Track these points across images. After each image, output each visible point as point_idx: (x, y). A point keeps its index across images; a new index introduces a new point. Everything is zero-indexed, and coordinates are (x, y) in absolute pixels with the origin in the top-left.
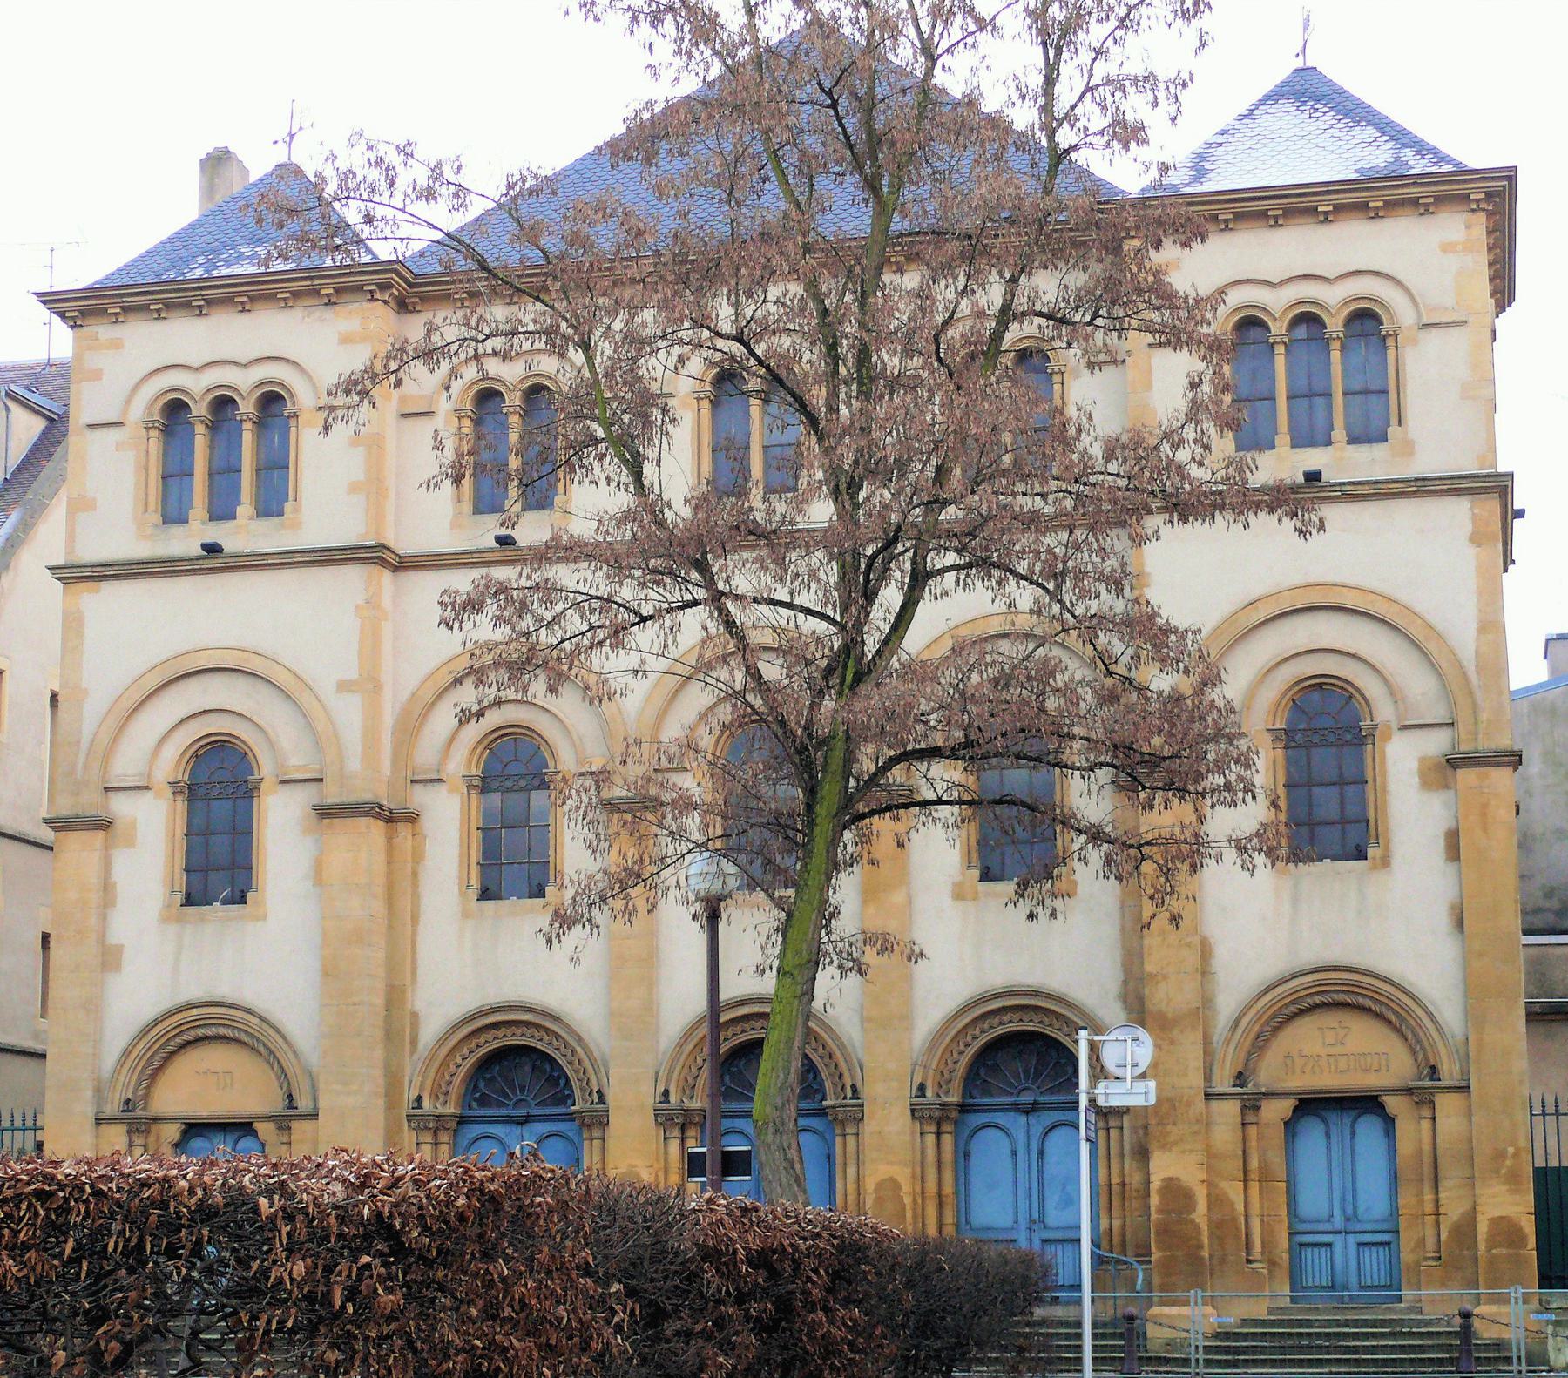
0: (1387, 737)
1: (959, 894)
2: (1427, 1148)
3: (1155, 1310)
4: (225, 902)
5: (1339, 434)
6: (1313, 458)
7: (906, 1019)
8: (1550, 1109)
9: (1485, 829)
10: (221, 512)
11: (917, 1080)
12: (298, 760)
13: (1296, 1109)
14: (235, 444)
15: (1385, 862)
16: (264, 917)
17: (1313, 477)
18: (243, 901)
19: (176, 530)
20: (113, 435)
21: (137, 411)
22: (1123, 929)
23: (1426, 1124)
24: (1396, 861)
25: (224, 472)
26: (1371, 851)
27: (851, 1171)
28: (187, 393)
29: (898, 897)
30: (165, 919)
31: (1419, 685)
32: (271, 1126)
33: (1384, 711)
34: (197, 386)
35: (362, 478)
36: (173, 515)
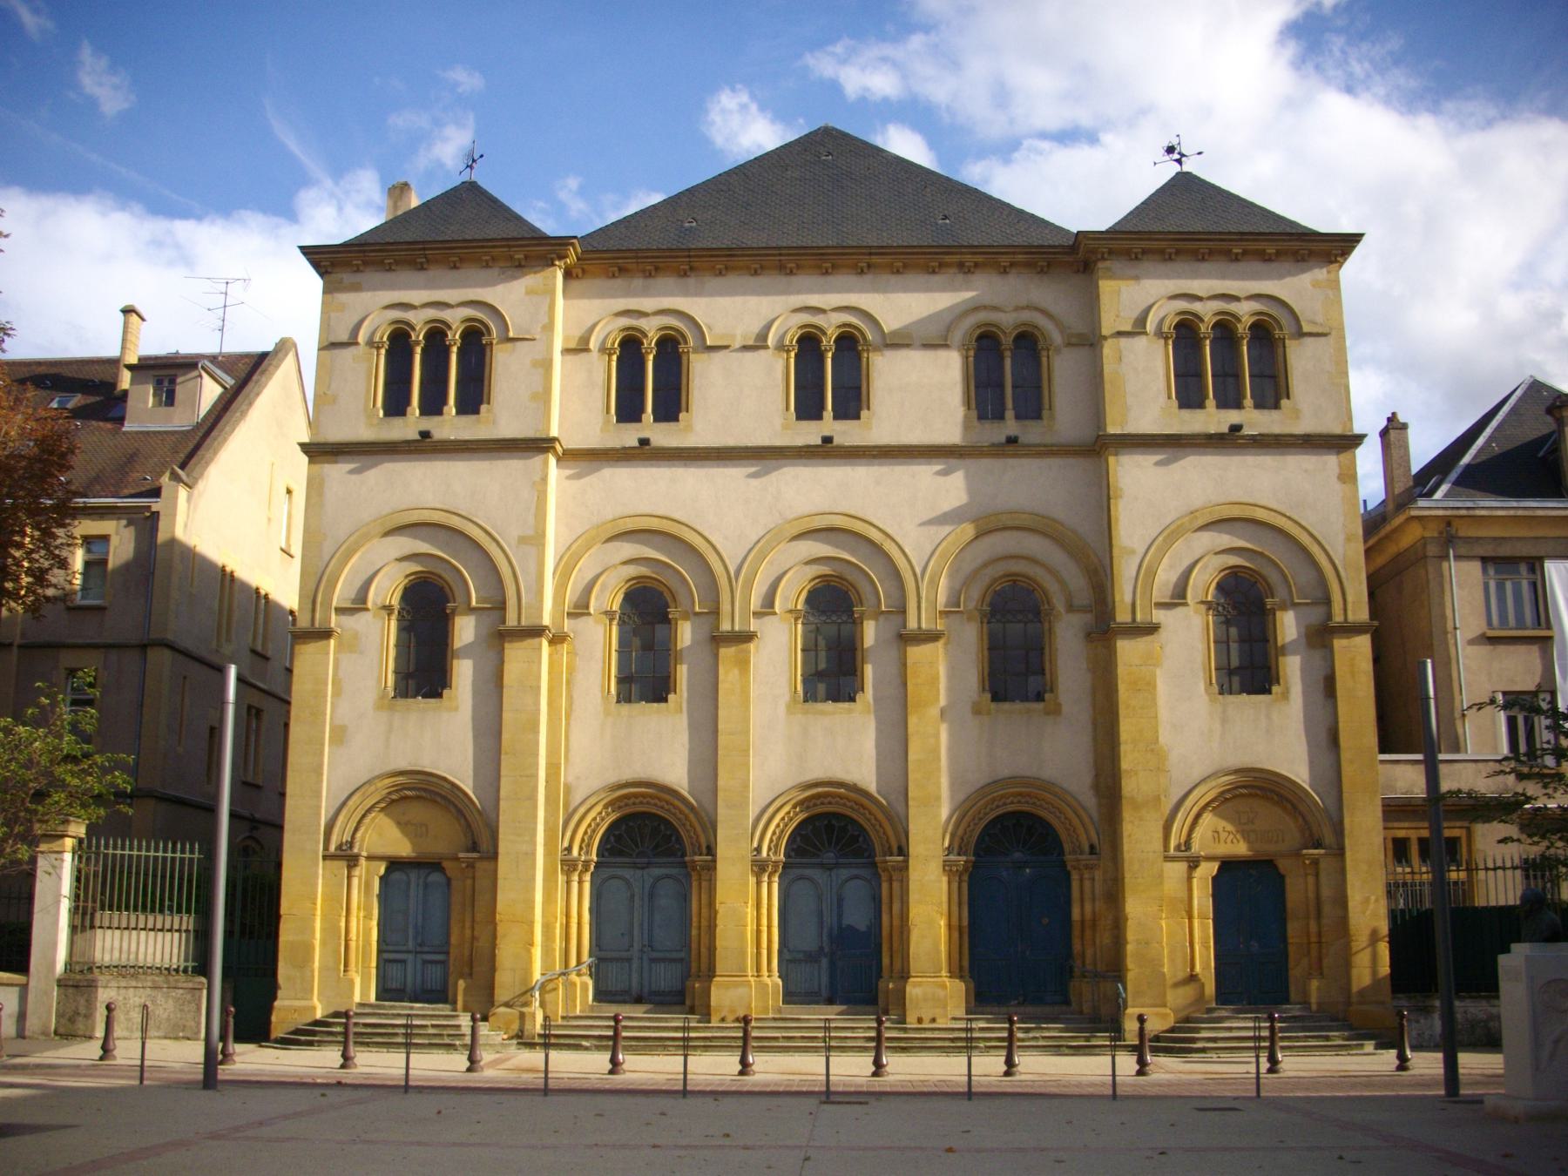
26: (1275, 689)
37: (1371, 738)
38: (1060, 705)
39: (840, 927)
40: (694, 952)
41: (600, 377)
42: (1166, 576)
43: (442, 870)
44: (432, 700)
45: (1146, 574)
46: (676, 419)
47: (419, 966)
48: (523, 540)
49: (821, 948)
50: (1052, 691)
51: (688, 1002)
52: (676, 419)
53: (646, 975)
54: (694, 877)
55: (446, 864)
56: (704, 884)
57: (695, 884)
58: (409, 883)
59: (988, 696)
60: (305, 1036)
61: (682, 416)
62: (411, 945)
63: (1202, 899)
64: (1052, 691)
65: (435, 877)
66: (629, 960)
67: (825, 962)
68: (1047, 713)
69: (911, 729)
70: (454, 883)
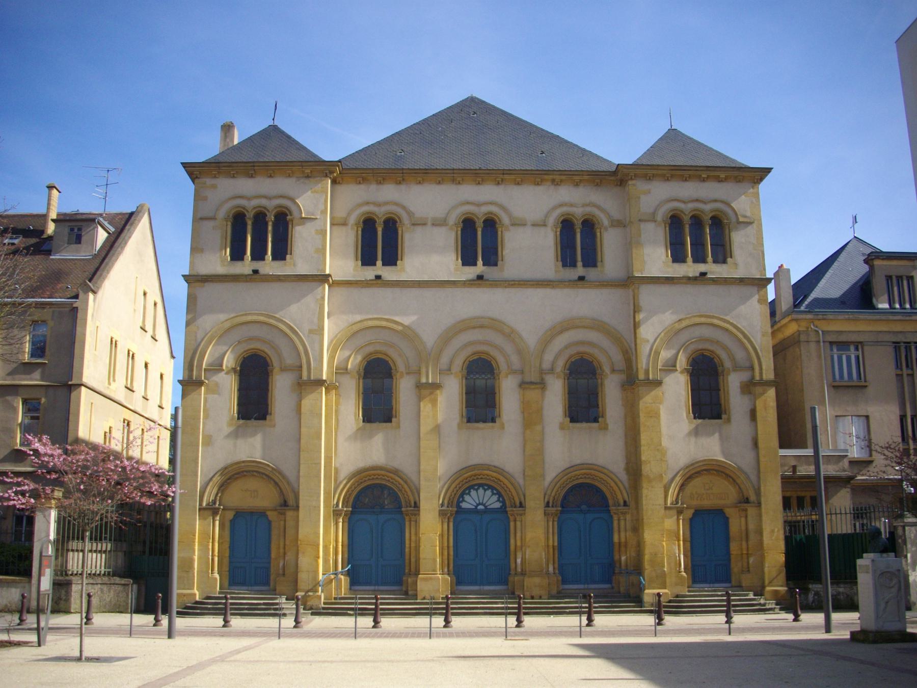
0: (728, 374)
1: (562, 427)
2: (743, 528)
3: (622, 589)
4: (256, 419)
5: (710, 259)
6: (702, 268)
7: (543, 476)
8: (843, 512)
9: (765, 409)
10: (258, 255)
11: (546, 500)
12: (289, 361)
13: (694, 514)
14: (703, 233)
15: (729, 420)
16: (274, 426)
17: (703, 274)
18: (264, 418)
19: (239, 263)
20: (211, 224)
21: (221, 214)
22: (626, 443)
23: (743, 519)
24: (732, 420)
25: (699, 245)
26: (724, 416)
27: (519, 535)
28: (265, 208)
29: (538, 428)
30: (460, 427)
31: (740, 355)
32: (275, 513)
33: (728, 364)
34: (251, 206)
35: (634, 251)
36: (237, 255)
38: (607, 425)
48: (311, 331)
52: (395, 264)
55: (269, 513)
56: (413, 523)
57: (407, 524)
59: (568, 419)
68: (601, 429)
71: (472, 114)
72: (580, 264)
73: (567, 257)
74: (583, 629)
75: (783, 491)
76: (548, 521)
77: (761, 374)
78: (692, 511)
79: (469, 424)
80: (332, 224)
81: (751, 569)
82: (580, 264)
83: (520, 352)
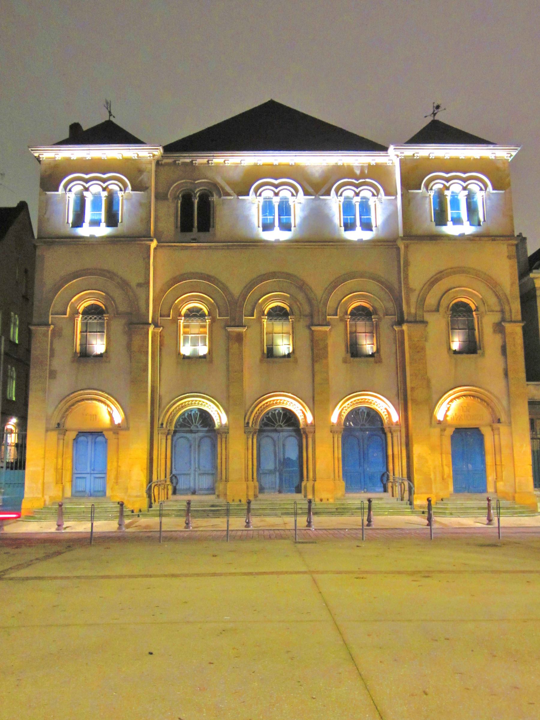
11: (246, 421)
15: (483, 354)
26: (479, 351)
37: (523, 375)
38: (381, 359)
39: (284, 459)
40: (219, 470)
41: (172, 211)
42: (431, 300)
43: (103, 436)
44: (472, 355)
45: (422, 300)
46: (208, 231)
47: (92, 480)
48: (139, 285)
49: (276, 468)
50: (480, 349)
51: (217, 493)
52: (208, 231)
53: (197, 481)
54: (219, 436)
55: (105, 433)
56: (224, 440)
57: (219, 440)
58: (88, 442)
59: (349, 355)
60: (31, 517)
61: (211, 229)
62: (89, 470)
63: (491, 477)
64: (480, 349)
65: (100, 439)
66: (189, 474)
67: (277, 474)
68: (376, 362)
69: (316, 370)
70: (109, 441)
71: (272, 109)
72: (195, 229)
73: (185, 226)
74: (365, 527)
75: (530, 414)
76: (248, 438)
77: (511, 316)
78: (453, 429)
79: (269, 359)
80: (156, 198)
81: (504, 478)
82: (195, 229)
83: (310, 301)
